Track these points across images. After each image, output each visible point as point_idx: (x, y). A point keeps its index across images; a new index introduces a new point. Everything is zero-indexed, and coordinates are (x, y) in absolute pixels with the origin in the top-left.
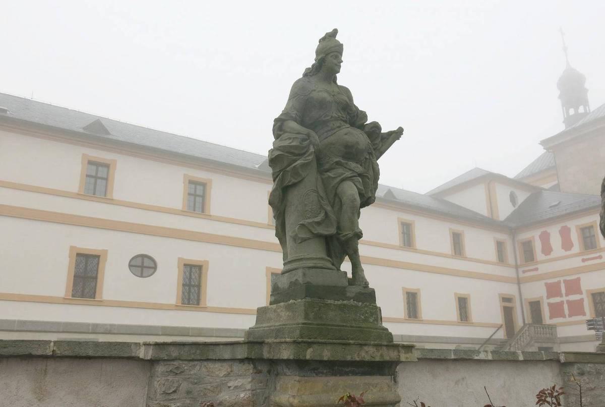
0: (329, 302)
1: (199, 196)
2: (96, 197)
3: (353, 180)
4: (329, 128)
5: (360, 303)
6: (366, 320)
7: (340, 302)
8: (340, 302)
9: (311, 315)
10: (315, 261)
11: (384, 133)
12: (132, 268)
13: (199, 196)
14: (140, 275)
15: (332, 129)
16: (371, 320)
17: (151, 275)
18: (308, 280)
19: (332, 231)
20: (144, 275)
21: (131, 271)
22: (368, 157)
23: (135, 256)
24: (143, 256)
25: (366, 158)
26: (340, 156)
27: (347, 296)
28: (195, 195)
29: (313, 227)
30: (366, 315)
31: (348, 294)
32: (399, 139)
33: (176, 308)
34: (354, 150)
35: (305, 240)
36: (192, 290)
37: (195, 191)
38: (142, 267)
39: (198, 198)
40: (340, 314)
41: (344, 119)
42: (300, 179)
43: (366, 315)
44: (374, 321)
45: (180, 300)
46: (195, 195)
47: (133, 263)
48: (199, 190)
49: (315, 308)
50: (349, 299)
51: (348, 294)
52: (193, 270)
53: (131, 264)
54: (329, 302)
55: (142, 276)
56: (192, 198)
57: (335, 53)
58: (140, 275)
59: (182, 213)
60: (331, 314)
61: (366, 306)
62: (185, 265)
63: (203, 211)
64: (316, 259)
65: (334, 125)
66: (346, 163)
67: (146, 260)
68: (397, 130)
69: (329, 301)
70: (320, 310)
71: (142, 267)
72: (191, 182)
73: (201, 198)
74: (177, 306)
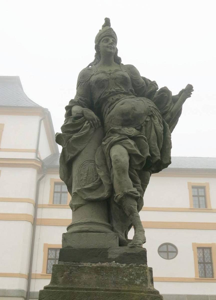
0: (85, 264)
1: (202, 196)
2: (61, 205)
3: (121, 143)
4: (110, 104)
5: (124, 265)
6: (131, 282)
7: (99, 264)
8: (99, 264)
9: (60, 279)
10: (81, 226)
11: (174, 96)
12: (160, 253)
13: (202, 196)
14: (167, 258)
15: (112, 104)
16: (138, 283)
17: (174, 257)
18: (69, 244)
19: (105, 194)
20: (170, 258)
21: (160, 256)
22: (148, 120)
23: (161, 245)
24: (167, 244)
25: (147, 122)
26: (119, 125)
27: (109, 258)
28: (198, 196)
29: (83, 194)
30: (131, 277)
31: (110, 256)
32: (190, 96)
33: (196, 280)
34: (130, 116)
35: (78, 207)
36: (207, 267)
37: (198, 193)
38: (167, 252)
39: (201, 198)
40: (96, 277)
41: (123, 92)
42: (76, 153)
43: (131, 277)
44: (141, 283)
45: (198, 275)
46: (198, 196)
47: (161, 250)
48: (201, 192)
49: (65, 271)
50: (110, 260)
51: (110, 256)
52: (206, 251)
53: (160, 250)
54: (85, 264)
55: (168, 259)
56: (197, 198)
57: (107, 37)
58: (167, 258)
59: (191, 210)
60: (85, 277)
61: (131, 267)
62: (198, 248)
63: (206, 207)
64: (85, 223)
65: (113, 99)
66: (120, 130)
67: (169, 246)
68: (185, 88)
69: (85, 264)
70: (71, 273)
71: (167, 252)
72: (193, 187)
73: (203, 198)
74: (196, 279)
